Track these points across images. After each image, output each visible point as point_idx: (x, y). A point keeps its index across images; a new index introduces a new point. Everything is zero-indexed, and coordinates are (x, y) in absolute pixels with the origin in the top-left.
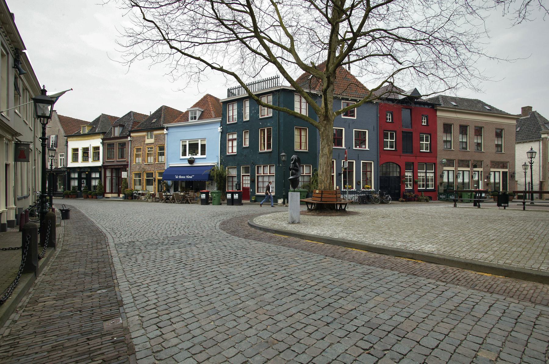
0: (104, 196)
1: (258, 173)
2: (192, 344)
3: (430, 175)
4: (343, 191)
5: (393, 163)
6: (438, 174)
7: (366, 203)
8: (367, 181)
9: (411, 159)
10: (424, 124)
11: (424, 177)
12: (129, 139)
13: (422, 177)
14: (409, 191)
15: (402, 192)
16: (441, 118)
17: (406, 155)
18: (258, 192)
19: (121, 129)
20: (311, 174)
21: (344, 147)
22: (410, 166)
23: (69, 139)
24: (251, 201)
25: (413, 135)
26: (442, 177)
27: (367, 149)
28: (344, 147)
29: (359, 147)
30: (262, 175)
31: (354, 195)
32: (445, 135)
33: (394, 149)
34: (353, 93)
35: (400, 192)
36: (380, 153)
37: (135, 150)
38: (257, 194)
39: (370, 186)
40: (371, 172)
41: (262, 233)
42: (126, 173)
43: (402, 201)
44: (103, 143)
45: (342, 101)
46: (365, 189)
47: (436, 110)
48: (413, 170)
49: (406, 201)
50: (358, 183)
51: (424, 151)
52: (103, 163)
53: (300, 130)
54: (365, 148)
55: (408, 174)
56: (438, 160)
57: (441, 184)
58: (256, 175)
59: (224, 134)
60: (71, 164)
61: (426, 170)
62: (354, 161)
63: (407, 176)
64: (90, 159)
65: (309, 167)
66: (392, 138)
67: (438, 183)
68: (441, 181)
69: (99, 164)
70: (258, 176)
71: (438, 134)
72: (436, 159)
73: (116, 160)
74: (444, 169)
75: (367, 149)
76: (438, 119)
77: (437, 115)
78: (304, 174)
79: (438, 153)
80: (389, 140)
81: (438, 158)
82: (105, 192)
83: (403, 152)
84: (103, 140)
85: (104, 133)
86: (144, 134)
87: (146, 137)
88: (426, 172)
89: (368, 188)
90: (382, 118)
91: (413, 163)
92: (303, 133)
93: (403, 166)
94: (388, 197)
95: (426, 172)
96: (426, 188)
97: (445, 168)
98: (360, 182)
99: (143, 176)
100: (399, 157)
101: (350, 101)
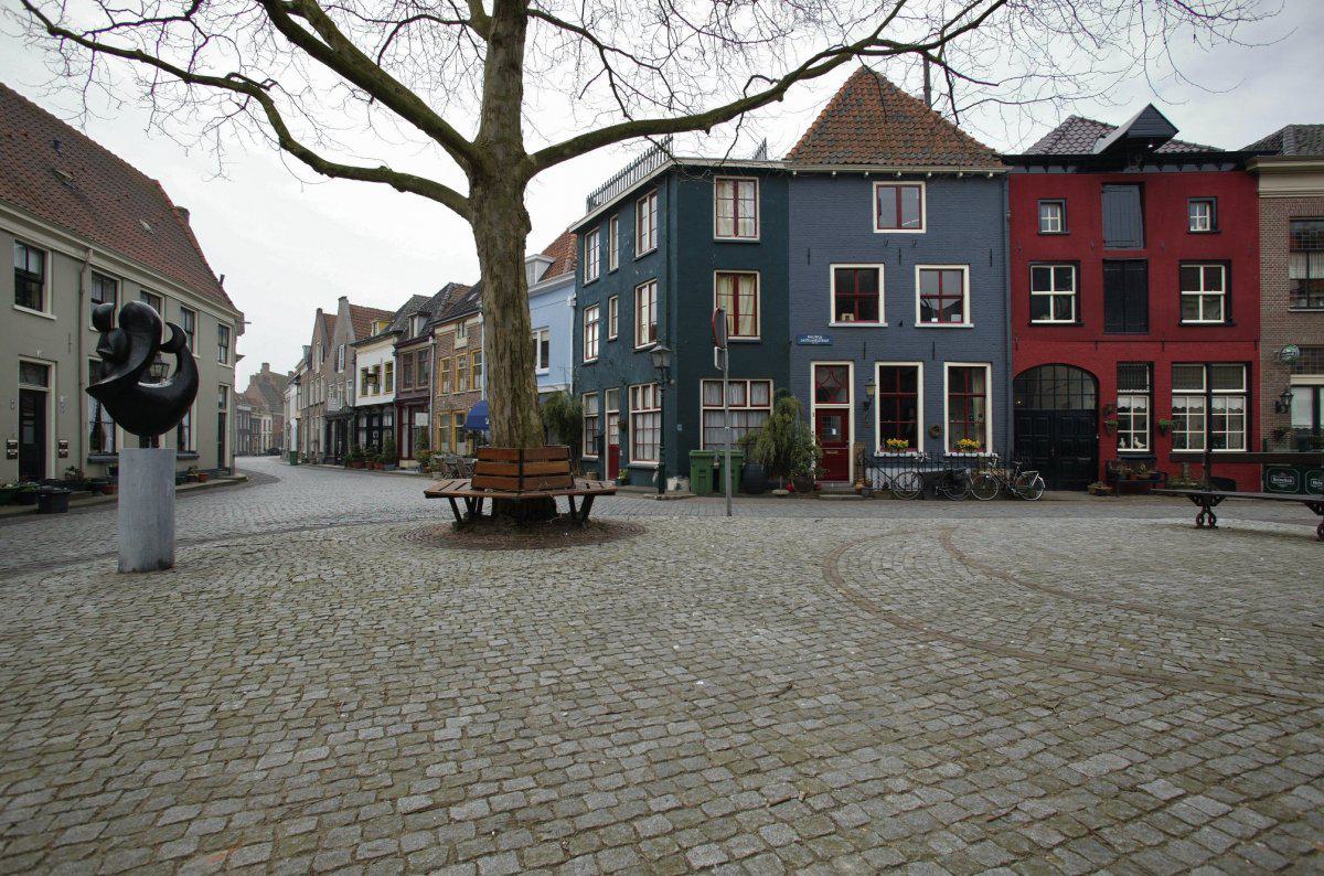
0: (398, 465)
1: (635, 408)
2: (680, 804)
3: (1230, 403)
4: (879, 458)
5: (1069, 366)
6: (1266, 399)
7: (942, 497)
8: (966, 420)
9: (1138, 349)
10: (1199, 229)
11: (1201, 410)
12: (431, 341)
13: (1192, 410)
14: (1133, 459)
15: (1102, 465)
16: (1278, 199)
17: (1123, 338)
18: (635, 458)
19: (423, 321)
20: (771, 408)
21: (882, 322)
22: (1131, 375)
23: (358, 351)
24: (792, 490)
25: (1151, 270)
26: (1282, 408)
27: (967, 323)
28: (882, 322)
29: (940, 321)
30: (652, 410)
31: (902, 470)
32: (1301, 259)
33: (1072, 321)
34: (913, 155)
35: (1095, 461)
36: (1014, 335)
37: (442, 365)
38: (633, 463)
39: (976, 444)
40: (984, 396)
41: (1010, 569)
42: (426, 415)
43: (1100, 493)
44: (396, 354)
45: (875, 184)
46: (958, 451)
47: (1255, 176)
48: (1152, 387)
49: (1114, 493)
50: (934, 433)
51: (1201, 321)
52: (397, 395)
53: (736, 279)
54: (962, 321)
55: (1133, 402)
56: (1265, 351)
57: (1279, 435)
58: (631, 411)
59: (580, 310)
60: (361, 402)
61: (1209, 388)
62: (920, 366)
63: (1128, 410)
64: (382, 389)
65: (765, 386)
66: (1063, 283)
67: (1265, 431)
68: (1277, 424)
69: (390, 398)
70: (634, 415)
71: (1265, 256)
72: (1256, 349)
73: (413, 392)
74: (1293, 382)
75: (967, 323)
76: (1262, 205)
77: (1258, 194)
78: (749, 407)
79: (1265, 326)
80: (1052, 292)
81: (1261, 346)
82: (400, 457)
83: (1108, 329)
84: (397, 346)
85: (397, 333)
86: (453, 327)
87: (456, 334)
88: (1209, 396)
89: (970, 449)
90: (1021, 222)
91: (1151, 365)
92: (745, 288)
93: (1108, 377)
94: (1031, 477)
95: (1209, 396)
96: (1210, 446)
97: (1296, 379)
98: (939, 429)
99: (451, 422)
100: (1092, 345)
101: (902, 178)
